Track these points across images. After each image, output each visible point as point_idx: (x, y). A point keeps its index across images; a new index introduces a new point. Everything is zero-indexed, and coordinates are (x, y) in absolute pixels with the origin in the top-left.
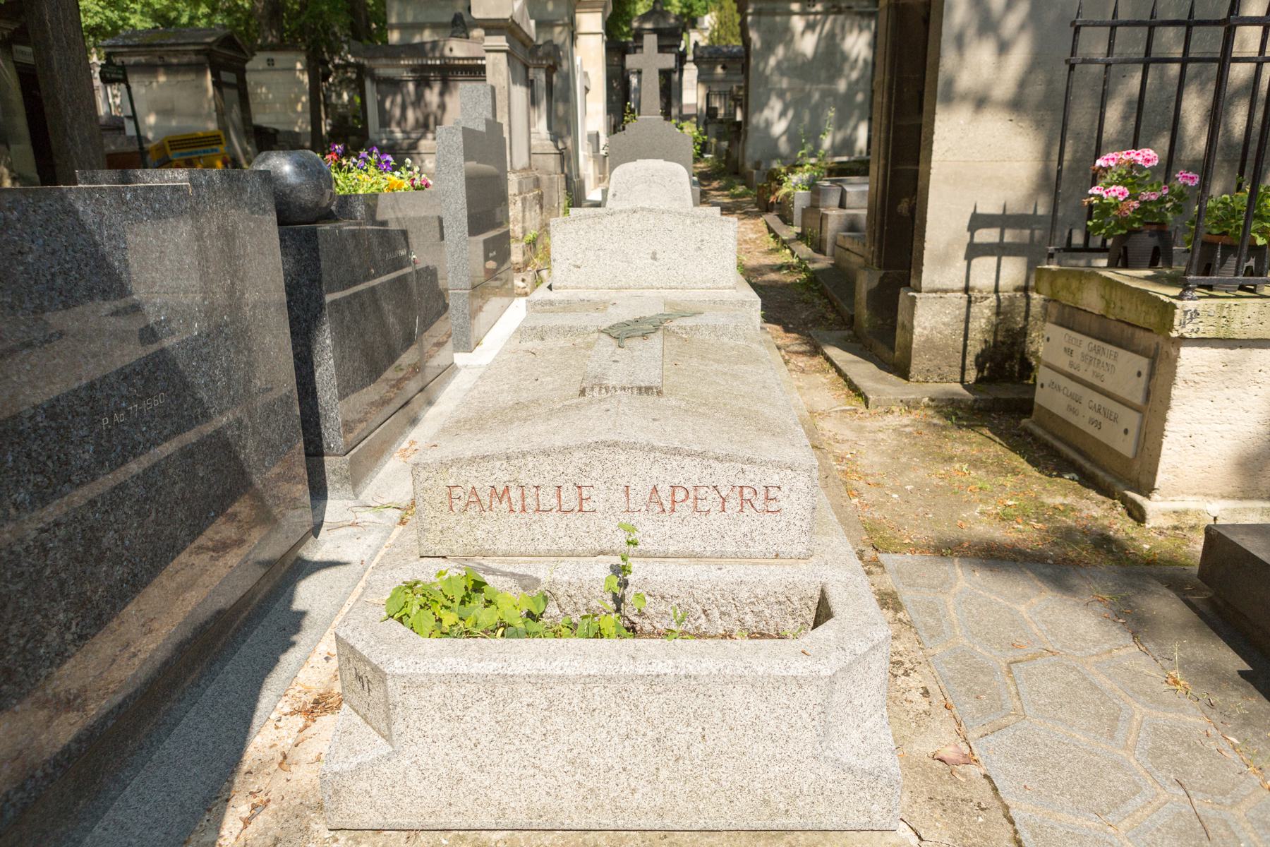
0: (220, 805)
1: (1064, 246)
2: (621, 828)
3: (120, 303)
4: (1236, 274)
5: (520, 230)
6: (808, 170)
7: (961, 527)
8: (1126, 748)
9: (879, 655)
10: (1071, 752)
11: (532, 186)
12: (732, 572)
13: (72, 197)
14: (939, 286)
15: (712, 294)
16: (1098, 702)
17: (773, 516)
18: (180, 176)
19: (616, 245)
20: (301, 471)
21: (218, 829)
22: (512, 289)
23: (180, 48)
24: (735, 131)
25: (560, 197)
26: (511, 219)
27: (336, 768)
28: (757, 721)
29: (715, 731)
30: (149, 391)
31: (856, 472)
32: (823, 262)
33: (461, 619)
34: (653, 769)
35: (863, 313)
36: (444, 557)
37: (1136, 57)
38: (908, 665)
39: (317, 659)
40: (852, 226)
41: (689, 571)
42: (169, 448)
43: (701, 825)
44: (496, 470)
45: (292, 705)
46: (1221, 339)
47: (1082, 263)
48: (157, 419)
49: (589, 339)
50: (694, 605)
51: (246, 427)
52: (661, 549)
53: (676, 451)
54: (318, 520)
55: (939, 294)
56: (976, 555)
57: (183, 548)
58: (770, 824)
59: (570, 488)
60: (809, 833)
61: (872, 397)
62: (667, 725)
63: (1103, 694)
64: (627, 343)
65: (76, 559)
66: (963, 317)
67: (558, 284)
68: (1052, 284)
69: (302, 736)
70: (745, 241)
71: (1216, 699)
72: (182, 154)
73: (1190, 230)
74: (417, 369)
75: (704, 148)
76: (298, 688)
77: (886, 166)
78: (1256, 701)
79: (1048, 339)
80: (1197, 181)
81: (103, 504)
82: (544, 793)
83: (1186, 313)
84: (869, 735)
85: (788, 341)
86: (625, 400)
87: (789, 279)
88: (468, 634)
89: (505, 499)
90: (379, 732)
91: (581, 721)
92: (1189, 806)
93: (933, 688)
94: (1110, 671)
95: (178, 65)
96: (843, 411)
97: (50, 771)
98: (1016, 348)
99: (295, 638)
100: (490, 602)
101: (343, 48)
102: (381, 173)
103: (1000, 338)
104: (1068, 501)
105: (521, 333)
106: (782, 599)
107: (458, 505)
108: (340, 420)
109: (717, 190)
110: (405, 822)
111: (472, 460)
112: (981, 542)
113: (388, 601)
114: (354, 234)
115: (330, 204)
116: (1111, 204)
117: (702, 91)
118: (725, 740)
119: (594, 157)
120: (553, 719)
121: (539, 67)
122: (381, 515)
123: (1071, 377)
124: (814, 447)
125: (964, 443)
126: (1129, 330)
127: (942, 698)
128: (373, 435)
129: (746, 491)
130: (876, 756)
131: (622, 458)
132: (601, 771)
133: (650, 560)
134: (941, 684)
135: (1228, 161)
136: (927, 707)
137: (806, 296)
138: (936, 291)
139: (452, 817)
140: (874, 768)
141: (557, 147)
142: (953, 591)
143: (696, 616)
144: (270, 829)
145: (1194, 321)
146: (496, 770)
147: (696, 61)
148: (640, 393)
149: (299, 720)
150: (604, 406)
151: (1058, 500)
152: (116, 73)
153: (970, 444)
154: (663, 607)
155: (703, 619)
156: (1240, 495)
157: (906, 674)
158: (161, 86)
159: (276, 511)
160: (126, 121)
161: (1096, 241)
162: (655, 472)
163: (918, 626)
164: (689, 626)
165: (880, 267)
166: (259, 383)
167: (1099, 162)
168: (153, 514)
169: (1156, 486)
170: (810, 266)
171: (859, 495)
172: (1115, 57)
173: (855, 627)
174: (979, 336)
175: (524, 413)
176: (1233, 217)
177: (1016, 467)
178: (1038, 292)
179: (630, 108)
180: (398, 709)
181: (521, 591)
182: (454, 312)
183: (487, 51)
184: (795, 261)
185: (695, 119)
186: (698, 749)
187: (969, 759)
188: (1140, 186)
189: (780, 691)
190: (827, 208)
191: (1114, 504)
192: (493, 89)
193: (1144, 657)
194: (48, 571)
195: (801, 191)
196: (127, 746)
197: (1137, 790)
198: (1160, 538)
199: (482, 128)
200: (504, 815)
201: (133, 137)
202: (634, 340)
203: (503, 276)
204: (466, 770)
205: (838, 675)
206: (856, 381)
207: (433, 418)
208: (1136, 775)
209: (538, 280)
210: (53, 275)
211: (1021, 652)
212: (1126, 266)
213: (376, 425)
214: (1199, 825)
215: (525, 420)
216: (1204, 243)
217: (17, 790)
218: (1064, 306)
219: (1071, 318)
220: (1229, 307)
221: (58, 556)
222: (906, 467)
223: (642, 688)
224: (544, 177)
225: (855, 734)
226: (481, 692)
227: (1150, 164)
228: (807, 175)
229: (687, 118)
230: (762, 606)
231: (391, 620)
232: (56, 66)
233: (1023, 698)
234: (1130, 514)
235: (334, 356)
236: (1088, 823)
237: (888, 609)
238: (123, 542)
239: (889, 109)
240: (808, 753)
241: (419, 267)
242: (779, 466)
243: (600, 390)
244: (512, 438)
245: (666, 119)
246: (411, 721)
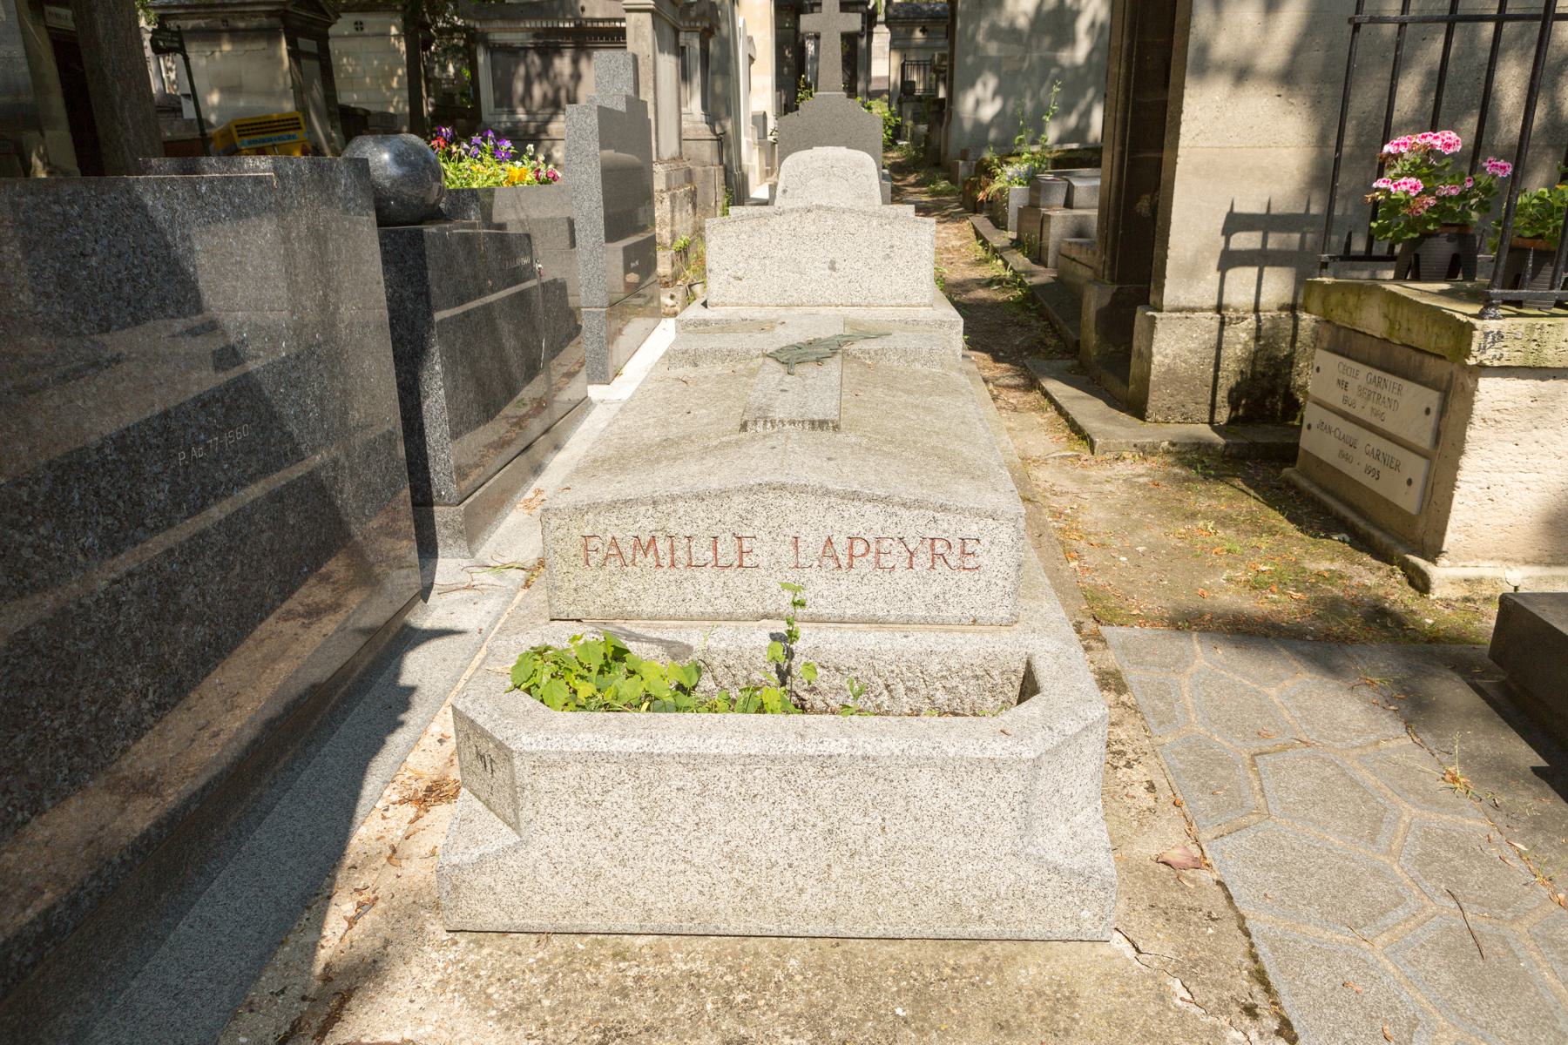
0: (321, 903)
1: (1342, 253)
2: (786, 934)
3: (197, 320)
4: (1552, 288)
5: (668, 235)
6: (1026, 160)
7: (1202, 596)
8: (1389, 853)
9: (1093, 737)
10: (1322, 857)
11: (682, 180)
12: (918, 642)
13: (139, 188)
14: (1184, 303)
15: (903, 313)
16: (1359, 801)
17: (970, 574)
18: (260, 166)
19: (786, 252)
20: (407, 524)
21: (319, 929)
22: (659, 308)
23: (247, 9)
24: (939, 112)
25: (717, 193)
26: (658, 220)
27: (455, 860)
28: (947, 811)
29: (897, 822)
30: (232, 421)
31: (1077, 530)
32: (1043, 276)
33: (599, 690)
34: (823, 865)
35: (1091, 338)
36: (579, 620)
37: (1440, 14)
38: (1131, 756)
39: (429, 741)
40: (1080, 232)
41: (869, 639)
42: (256, 491)
43: (880, 932)
44: (640, 517)
45: (401, 792)
46: (1529, 367)
47: (1365, 275)
48: (240, 455)
49: (752, 365)
50: (874, 678)
51: (343, 468)
52: (836, 612)
53: (855, 496)
54: (427, 582)
55: (1184, 314)
56: (1218, 629)
57: (273, 609)
58: (960, 932)
60: (1007, 943)
61: (1098, 441)
63: (1365, 792)
64: (798, 369)
65: (152, 615)
66: (1214, 342)
67: (715, 300)
68: (1324, 301)
69: (413, 828)
70: (947, 249)
71: (1502, 799)
72: (255, 142)
73: (1496, 232)
74: (541, 405)
75: (897, 132)
76: (408, 774)
77: (1122, 153)
78: (1550, 802)
79: (1318, 369)
80: (1509, 171)
81: (181, 553)
83: (1486, 335)
84: (1079, 830)
85: (997, 373)
86: (794, 435)
87: (1001, 297)
88: (607, 707)
89: (651, 552)
90: (504, 820)
92: (1460, 920)
93: (1160, 782)
94: (1376, 765)
95: (246, 30)
96: (1062, 457)
97: (128, 857)
98: (1279, 381)
99: (403, 717)
100: (632, 673)
101: (447, 7)
102: (499, 163)
103: (1259, 369)
104: (1336, 566)
105: (670, 357)
106: (979, 672)
107: (596, 558)
108: (452, 462)
109: (912, 185)
110: (535, 923)
111: (612, 506)
112: (1225, 615)
113: (513, 669)
114: (466, 239)
115: (439, 200)
116: (1400, 200)
117: (896, 60)
118: (909, 832)
119: (760, 144)
121: (691, 30)
122: (501, 578)
123: (1346, 416)
124: (1025, 499)
125: (1210, 497)
126: (1418, 357)
127: (1171, 794)
128: (491, 481)
129: (938, 544)
130: (1087, 855)
131: (791, 504)
132: (763, 868)
133: (823, 625)
134: (1170, 778)
135: (1554, 147)
136: (1152, 804)
137: (1022, 317)
138: (1180, 310)
139: (589, 919)
140: (1084, 869)
141: (714, 132)
142: (1189, 670)
143: (877, 692)
144: (380, 929)
145: (1497, 345)
146: (641, 864)
147: (887, 23)
148: (813, 428)
149: (410, 810)
150: (769, 444)
151: (1323, 566)
152: (172, 41)
153: (1219, 497)
154: (838, 681)
155: (885, 696)
156: (1548, 560)
157: (1129, 765)
158: (224, 56)
159: (377, 570)
160: (183, 100)
161: (1381, 248)
162: (830, 520)
163: (1145, 710)
164: (869, 703)
165: (1113, 281)
166: (357, 415)
167: (1387, 148)
168: (238, 567)
169: (1444, 549)
170: (1027, 281)
171: (1079, 557)
172: (1412, 14)
173: (1065, 704)
174: (1233, 366)
175: (673, 451)
176: (1551, 216)
177: (1274, 526)
178: (1307, 311)
179: (805, 83)
180: (527, 793)
181: (669, 661)
182: (588, 335)
183: (628, 11)
184: (1009, 273)
185: (886, 97)
186: (877, 843)
187: (1200, 863)
188: (1438, 177)
189: (974, 776)
190: (1049, 207)
191: (1392, 570)
192: (635, 58)
193: (1418, 750)
194: (121, 630)
195: (1017, 187)
196: (213, 835)
197: (1400, 901)
198: (1447, 611)
199: (622, 107)
201: (192, 120)
202: (806, 365)
203: (647, 291)
204: (606, 864)
205: (1044, 757)
206: (1080, 420)
207: (559, 465)
208: (1399, 883)
209: (690, 296)
210: (120, 281)
211: (1269, 742)
212: (1417, 278)
213: (494, 470)
214: (1471, 941)
215: (675, 459)
216: (1512, 249)
217: (92, 877)
218: (1339, 328)
219: (1345, 342)
220: (1542, 327)
221: (132, 611)
222: (1139, 525)
223: (811, 770)
224: (698, 170)
225: (1063, 829)
226: (623, 773)
227: (1451, 150)
228: (1026, 166)
229: (877, 94)
230: (955, 681)
231: (517, 691)
232: (101, 32)
233: (1268, 795)
234: (1411, 583)
235: (445, 386)
236: (1339, 937)
237: (1109, 690)
238: (204, 599)
239: (1127, 80)
240: (1007, 849)
241: (545, 279)
242: (978, 514)
243: (765, 424)
244: (659, 480)
245: (849, 97)
246: (542, 807)
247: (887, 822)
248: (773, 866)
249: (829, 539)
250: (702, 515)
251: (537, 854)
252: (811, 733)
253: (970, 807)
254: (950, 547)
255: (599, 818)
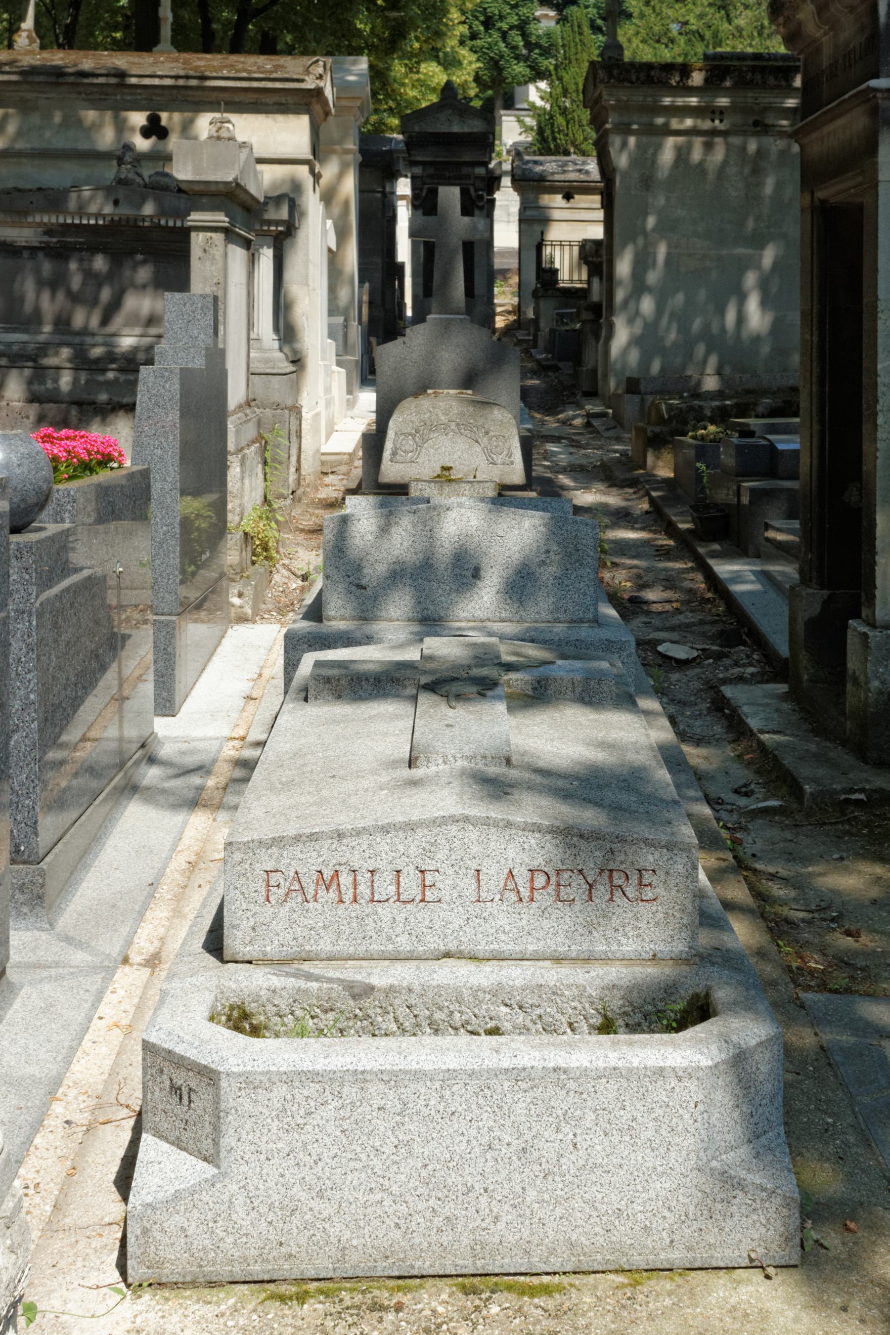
28: (634, 1124)
34: (518, 1189)
50: (558, 1016)
59: (412, 872)
62: (534, 1130)
82: (393, 1225)
91: (438, 1127)
107: (277, 894)
118: (598, 1148)
120: (406, 1127)
133: (505, 963)
146: (338, 1195)
180: (230, 1117)
189: (658, 1085)
200: (343, 1256)
204: (303, 1196)
223: (507, 1084)
226: (327, 1093)
247: (579, 1139)
248: (469, 1191)
249: (511, 872)
250: (387, 848)
251: (234, 1187)
252: (504, 1049)
253: (656, 1119)
254: (627, 878)
255: (300, 1144)
